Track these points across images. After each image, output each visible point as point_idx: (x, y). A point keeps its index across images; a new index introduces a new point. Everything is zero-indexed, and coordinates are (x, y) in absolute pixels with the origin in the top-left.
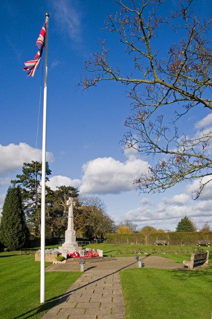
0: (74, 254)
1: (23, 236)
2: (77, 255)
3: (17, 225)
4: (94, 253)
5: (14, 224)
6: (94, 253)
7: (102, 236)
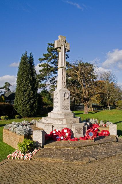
0: (62, 133)
1: (34, 103)
2: (67, 134)
3: (28, 92)
4: (101, 129)
5: (25, 91)
6: (101, 129)
7: (114, 104)
